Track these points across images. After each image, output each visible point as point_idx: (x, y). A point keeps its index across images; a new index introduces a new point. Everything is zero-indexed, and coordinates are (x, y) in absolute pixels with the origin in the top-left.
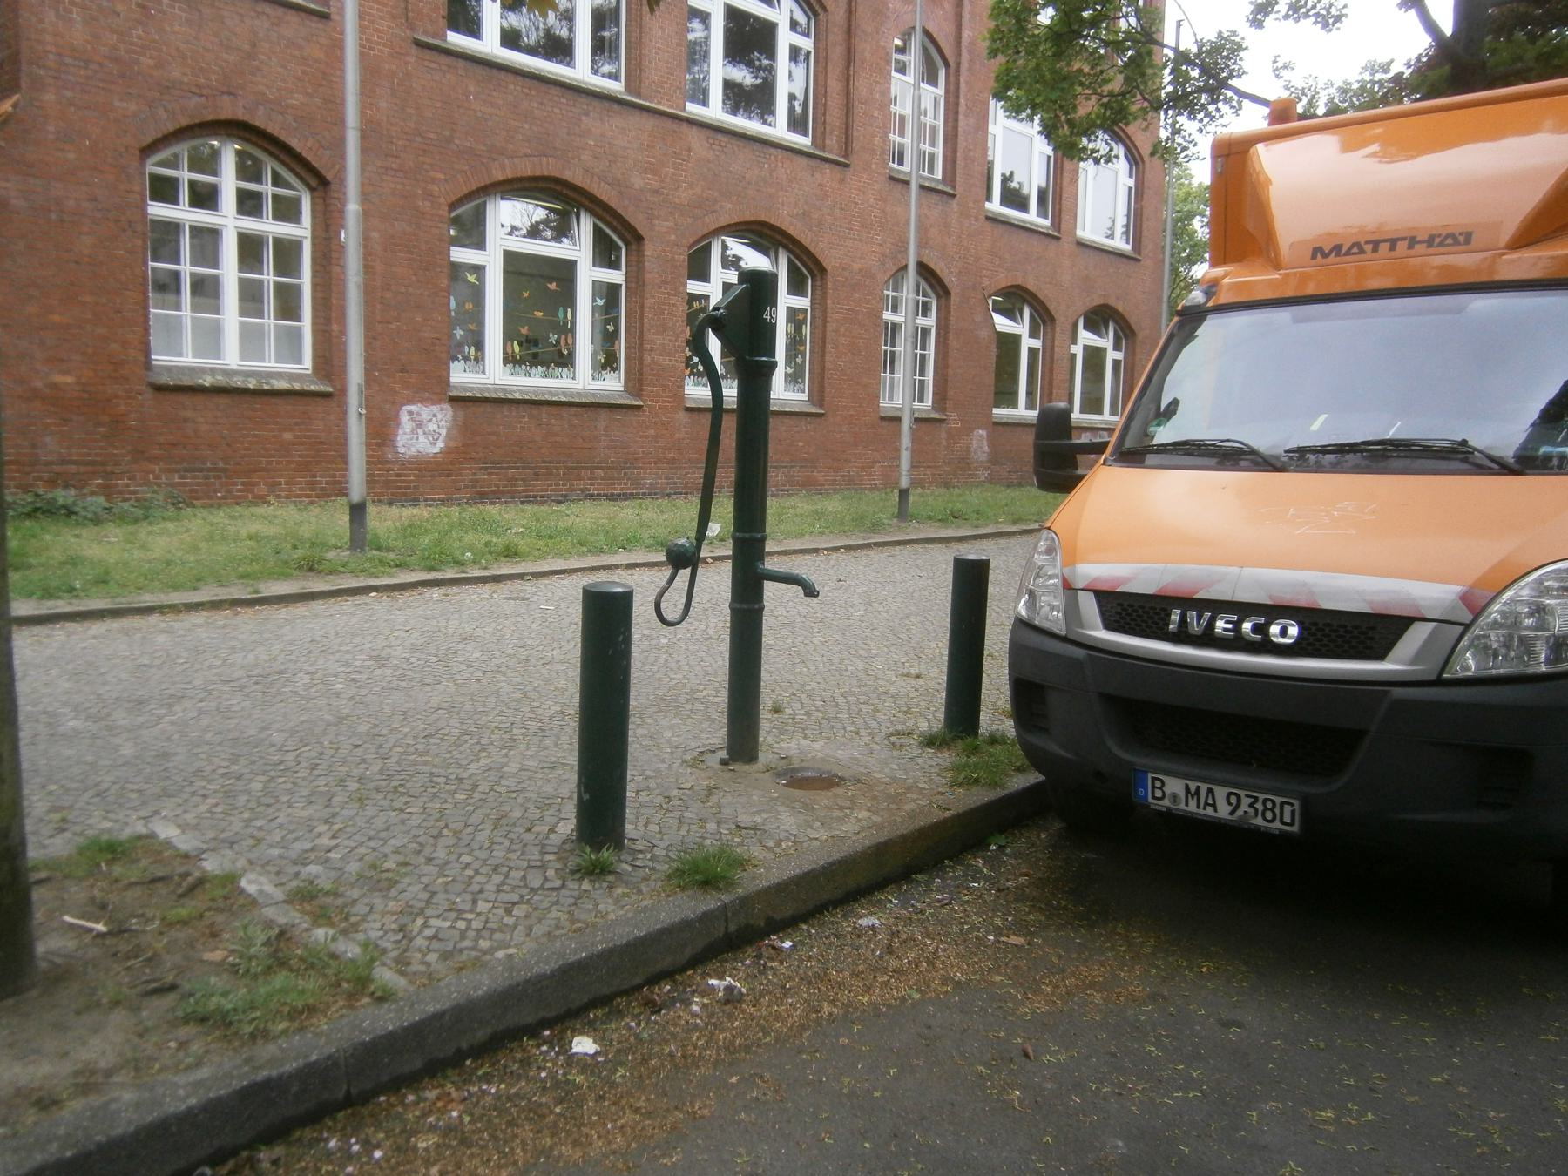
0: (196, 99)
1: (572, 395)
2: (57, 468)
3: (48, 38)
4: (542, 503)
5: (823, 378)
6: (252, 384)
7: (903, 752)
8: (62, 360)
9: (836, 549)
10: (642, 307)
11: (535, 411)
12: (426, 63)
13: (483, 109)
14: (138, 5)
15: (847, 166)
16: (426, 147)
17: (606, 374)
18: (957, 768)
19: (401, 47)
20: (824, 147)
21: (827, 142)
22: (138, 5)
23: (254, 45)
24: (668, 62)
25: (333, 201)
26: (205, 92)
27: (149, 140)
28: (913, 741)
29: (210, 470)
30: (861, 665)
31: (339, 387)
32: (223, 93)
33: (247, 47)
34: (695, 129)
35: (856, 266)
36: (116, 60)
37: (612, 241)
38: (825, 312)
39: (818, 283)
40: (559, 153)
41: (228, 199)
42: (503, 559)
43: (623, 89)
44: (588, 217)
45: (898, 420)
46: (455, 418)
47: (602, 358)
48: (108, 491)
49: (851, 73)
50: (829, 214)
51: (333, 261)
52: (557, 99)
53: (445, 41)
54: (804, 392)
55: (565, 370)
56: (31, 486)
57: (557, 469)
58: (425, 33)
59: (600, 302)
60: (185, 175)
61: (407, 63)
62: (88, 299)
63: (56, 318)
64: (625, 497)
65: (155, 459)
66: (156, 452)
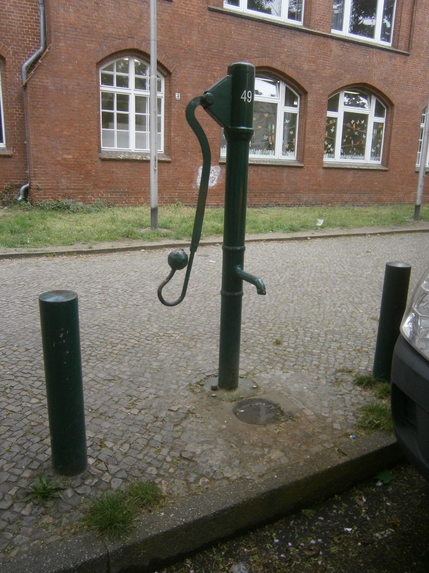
0: (118, 41)
1: (273, 162)
2: (66, 191)
3: (61, 20)
4: (257, 207)
5: (389, 154)
6: (139, 158)
7: (341, 388)
8: (68, 149)
9: (375, 234)
10: (306, 123)
11: (256, 169)
12: (214, 18)
13: (237, 37)
14: (95, 2)
15: (408, 55)
16: (212, 56)
17: (289, 153)
18: (371, 410)
19: (203, 12)
20: (398, 47)
21: (400, 44)
22: (95, 2)
23: (141, 16)
24: (323, 10)
25: (172, 81)
26: (121, 37)
27: (99, 59)
28: (350, 378)
29: (122, 192)
30: (351, 309)
31: (174, 159)
32: (129, 37)
33: (138, 17)
34: (334, 41)
35: (409, 103)
36: (87, 27)
37: (294, 95)
38: (392, 125)
39: (390, 111)
40: (271, 55)
41: (132, 83)
42: (214, 234)
43: (302, 25)
44: (283, 84)
45: (148, 161)
46: (221, 172)
47: (287, 146)
48: (84, 200)
49: (415, 10)
50: (397, 79)
51: (172, 106)
52: (271, 31)
53: (222, 8)
54: (379, 160)
55: (271, 151)
56: (57, 198)
57: (265, 193)
58: (214, 5)
59: (287, 122)
60: (115, 74)
61: (205, 19)
62: (77, 125)
63: (65, 133)
64: (294, 205)
65: (101, 188)
66: (102, 185)
